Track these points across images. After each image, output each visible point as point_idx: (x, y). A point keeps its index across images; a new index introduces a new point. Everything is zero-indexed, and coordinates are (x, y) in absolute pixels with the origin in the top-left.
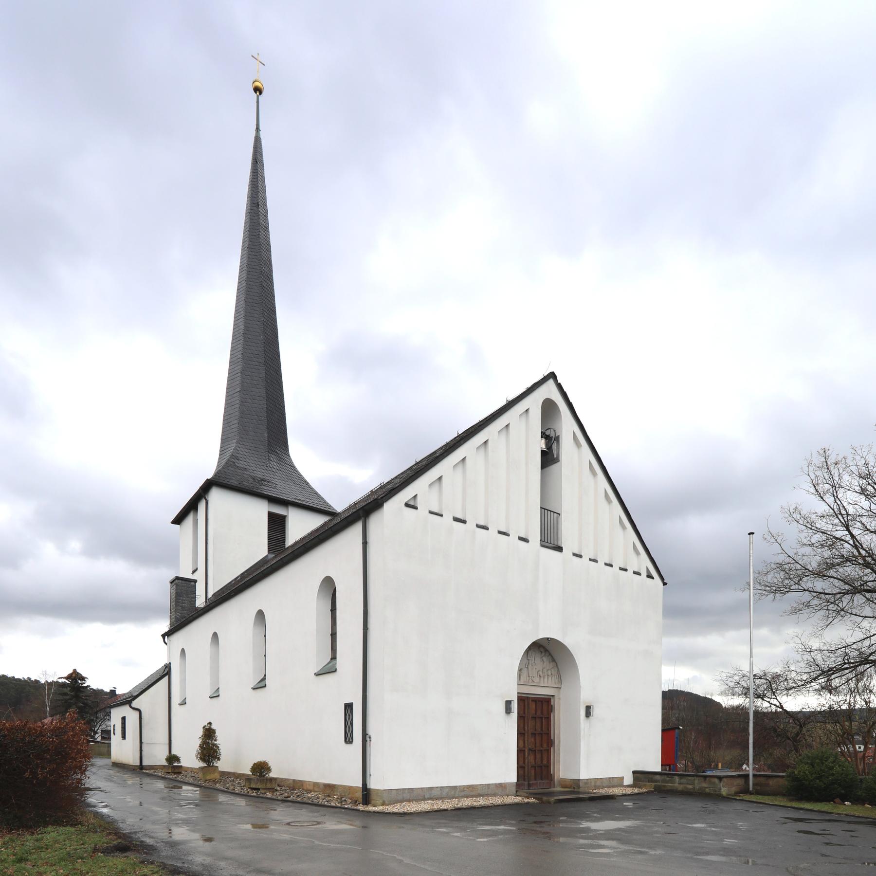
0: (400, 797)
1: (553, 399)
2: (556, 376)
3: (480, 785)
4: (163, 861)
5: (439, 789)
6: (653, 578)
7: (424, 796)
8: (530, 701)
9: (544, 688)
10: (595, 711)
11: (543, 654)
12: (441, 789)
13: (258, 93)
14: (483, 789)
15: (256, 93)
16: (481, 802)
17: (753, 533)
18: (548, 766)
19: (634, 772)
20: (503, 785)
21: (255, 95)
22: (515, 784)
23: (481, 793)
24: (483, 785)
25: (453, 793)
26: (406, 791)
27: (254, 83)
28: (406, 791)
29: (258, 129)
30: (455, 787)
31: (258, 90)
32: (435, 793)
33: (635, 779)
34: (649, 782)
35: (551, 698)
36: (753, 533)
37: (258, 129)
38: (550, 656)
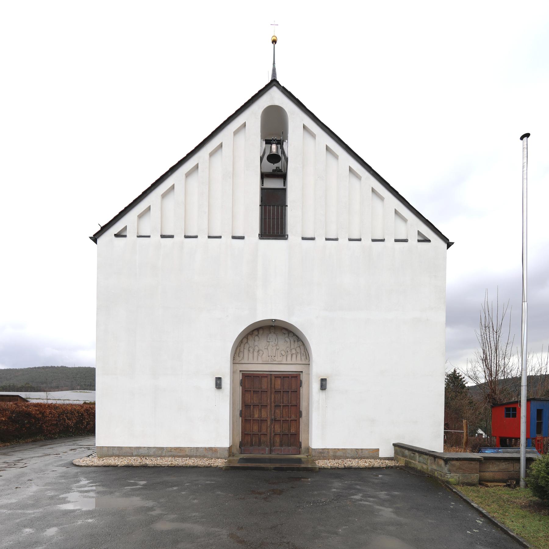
0: (111, 453)
1: (277, 103)
2: (278, 82)
3: (188, 448)
4: (45, 482)
5: (146, 449)
6: (429, 241)
7: (132, 453)
8: (273, 378)
9: (246, 364)
10: (329, 385)
11: (287, 335)
12: (148, 449)
13: (274, 43)
14: (191, 452)
15: (273, 44)
16: (190, 462)
17: (527, 135)
18: (296, 435)
19: (394, 445)
20: (214, 450)
21: (273, 45)
22: (228, 449)
23: (188, 454)
24: (191, 448)
25: (160, 452)
26: (116, 449)
27: (272, 37)
28: (116, 449)
29: (274, 63)
30: (162, 449)
31: (274, 42)
32: (142, 452)
33: (396, 452)
34: (402, 457)
35: (300, 374)
36: (527, 135)
37: (274, 63)
38: (295, 337)
